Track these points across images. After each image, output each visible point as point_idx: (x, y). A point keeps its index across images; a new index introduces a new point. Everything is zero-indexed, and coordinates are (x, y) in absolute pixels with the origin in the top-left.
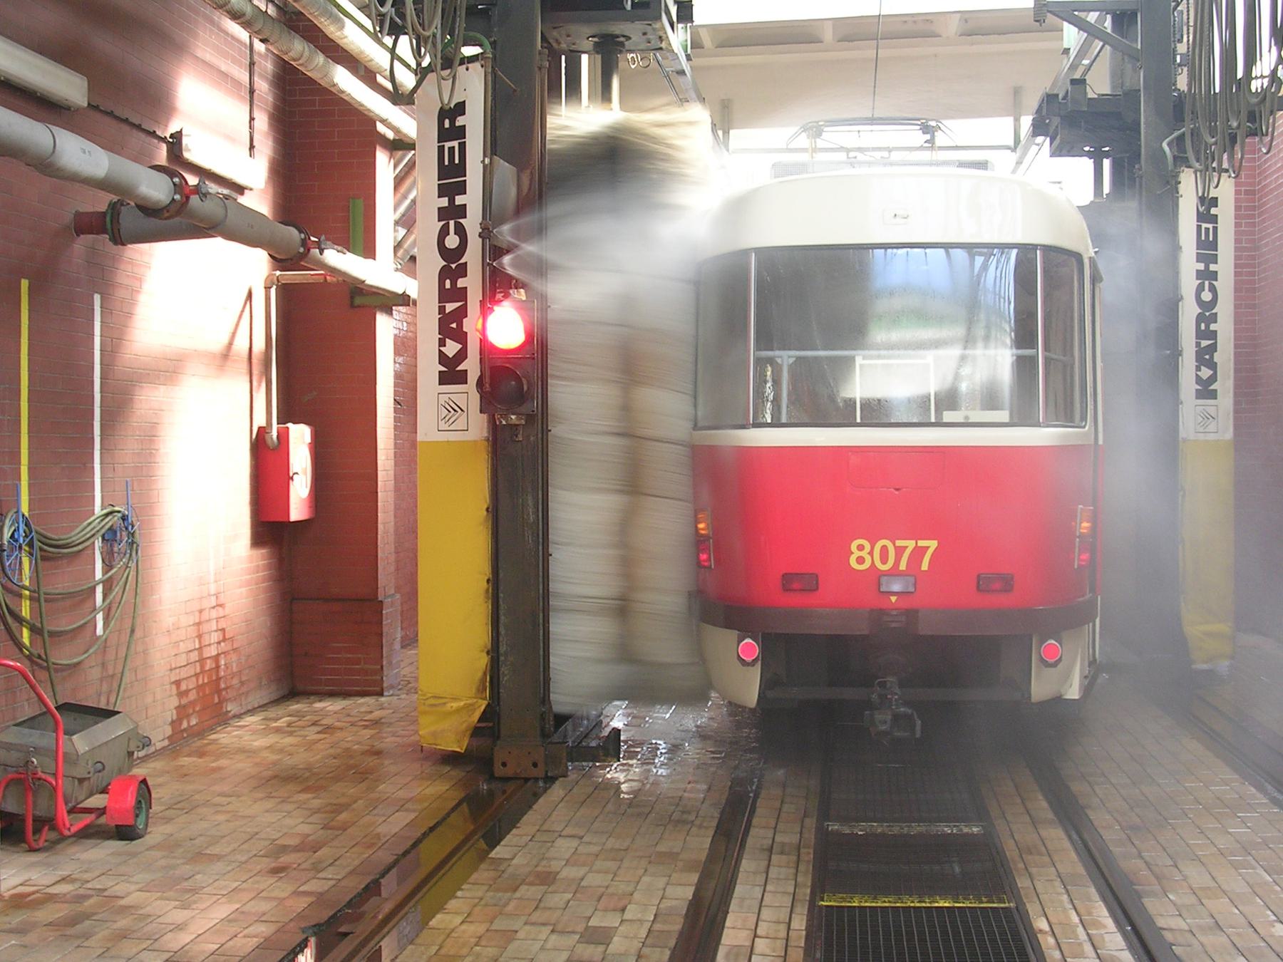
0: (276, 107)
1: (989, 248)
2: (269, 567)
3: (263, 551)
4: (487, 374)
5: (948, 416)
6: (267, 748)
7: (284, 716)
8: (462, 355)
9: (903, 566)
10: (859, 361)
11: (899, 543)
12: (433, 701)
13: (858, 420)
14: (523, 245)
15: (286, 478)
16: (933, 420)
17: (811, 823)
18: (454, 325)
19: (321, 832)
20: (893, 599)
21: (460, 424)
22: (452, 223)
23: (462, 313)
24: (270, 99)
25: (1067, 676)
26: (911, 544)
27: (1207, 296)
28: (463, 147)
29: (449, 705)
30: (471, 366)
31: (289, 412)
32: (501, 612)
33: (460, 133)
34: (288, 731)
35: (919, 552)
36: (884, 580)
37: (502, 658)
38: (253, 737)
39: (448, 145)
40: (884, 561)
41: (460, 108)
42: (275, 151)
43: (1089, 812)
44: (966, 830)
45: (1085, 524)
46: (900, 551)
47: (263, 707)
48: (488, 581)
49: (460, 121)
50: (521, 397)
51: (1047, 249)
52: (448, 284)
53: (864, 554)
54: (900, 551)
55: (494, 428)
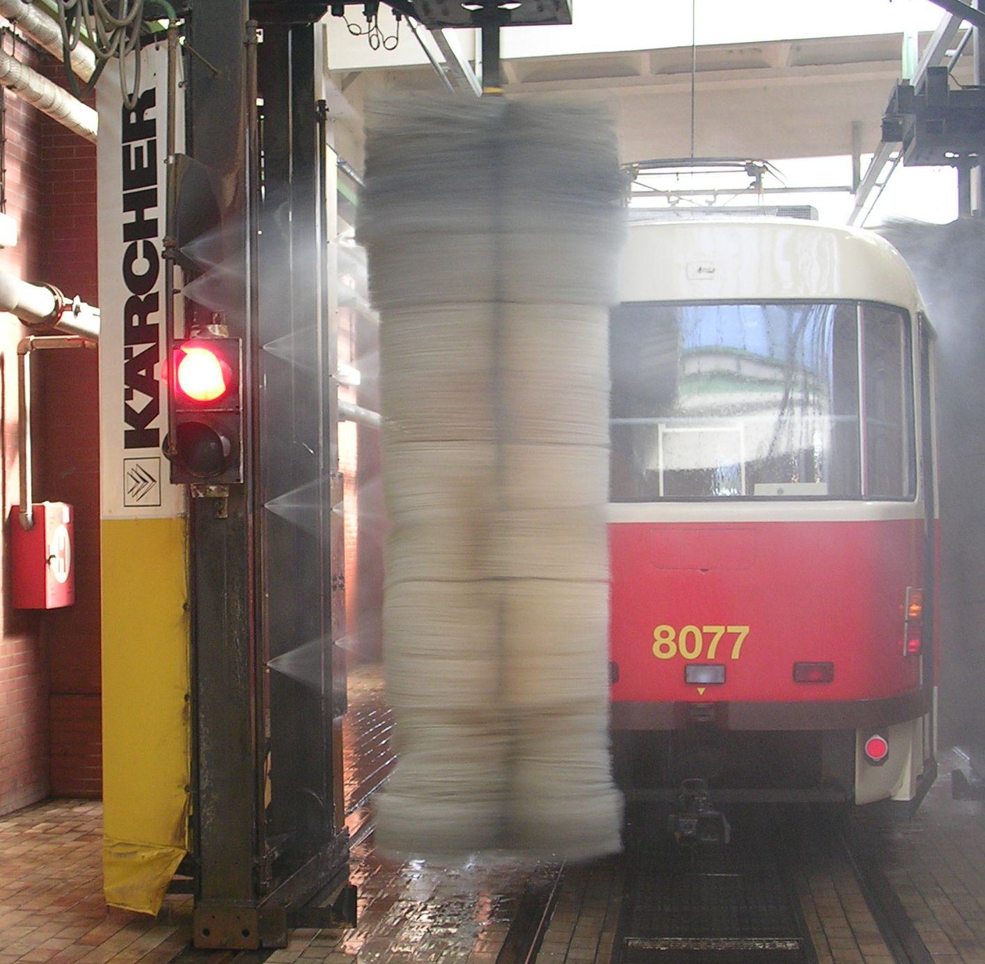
0: (30, 158)
1: (808, 303)
2: (24, 659)
3: (17, 642)
4: (173, 432)
5: (760, 490)
6: (19, 857)
7: (39, 822)
8: (152, 411)
9: (711, 655)
10: (662, 429)
11: (707, 629)
12: (119, 850)
13: (662, 494)
14: (218, 267)
15: (43, 561)
16: (743, 494)
17: (609, 936)
18: (143, 373)
19: (72, 947)
20: (701, 691)
21: (152, 498)
22: (140, 243)
23: (151, 357)
24: (23, 148)
25: (896, 776)
26: (719, 630)
27: (141, 266)
28: (152, 146)
29: (141, 854)
30: (161, 423)
31: (45, 489)
32: (202, 737)
33: (148, 129)
34: (46, 836)
35: (729, 640)
36: (690, 669)
37: (204, 796)
38: (5, 845)
39: (134, 144)
40: (691, 648)
41: (149, 99)
42: (29, 205)
43: (918, 926)
44: (779, 945)
45: (914, 608)
46: (708, 638)
47: (18, 812)
48: (186, 697)
49: (149, 114)
50: (224, 463)
51: (869, 305)
52: (136, 321)
53: (669, 641)
54: (708, 638)
55: (193, 505)
